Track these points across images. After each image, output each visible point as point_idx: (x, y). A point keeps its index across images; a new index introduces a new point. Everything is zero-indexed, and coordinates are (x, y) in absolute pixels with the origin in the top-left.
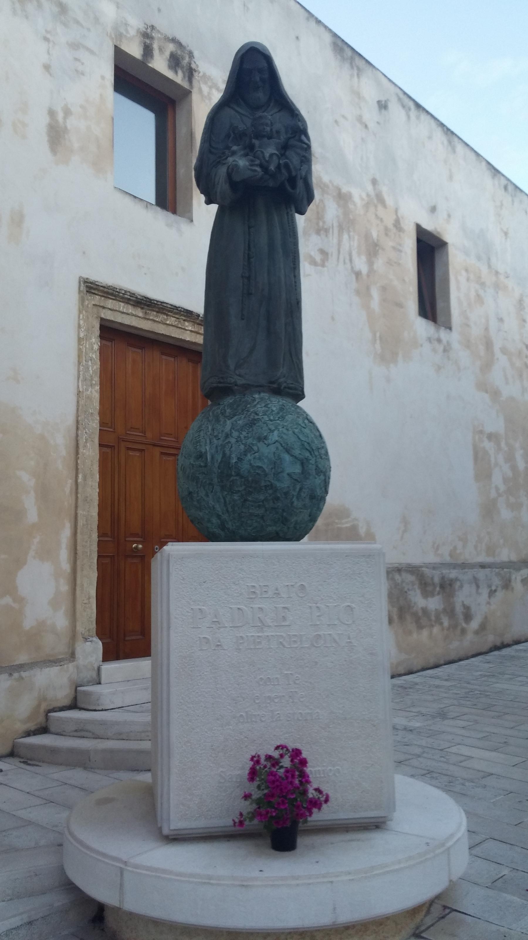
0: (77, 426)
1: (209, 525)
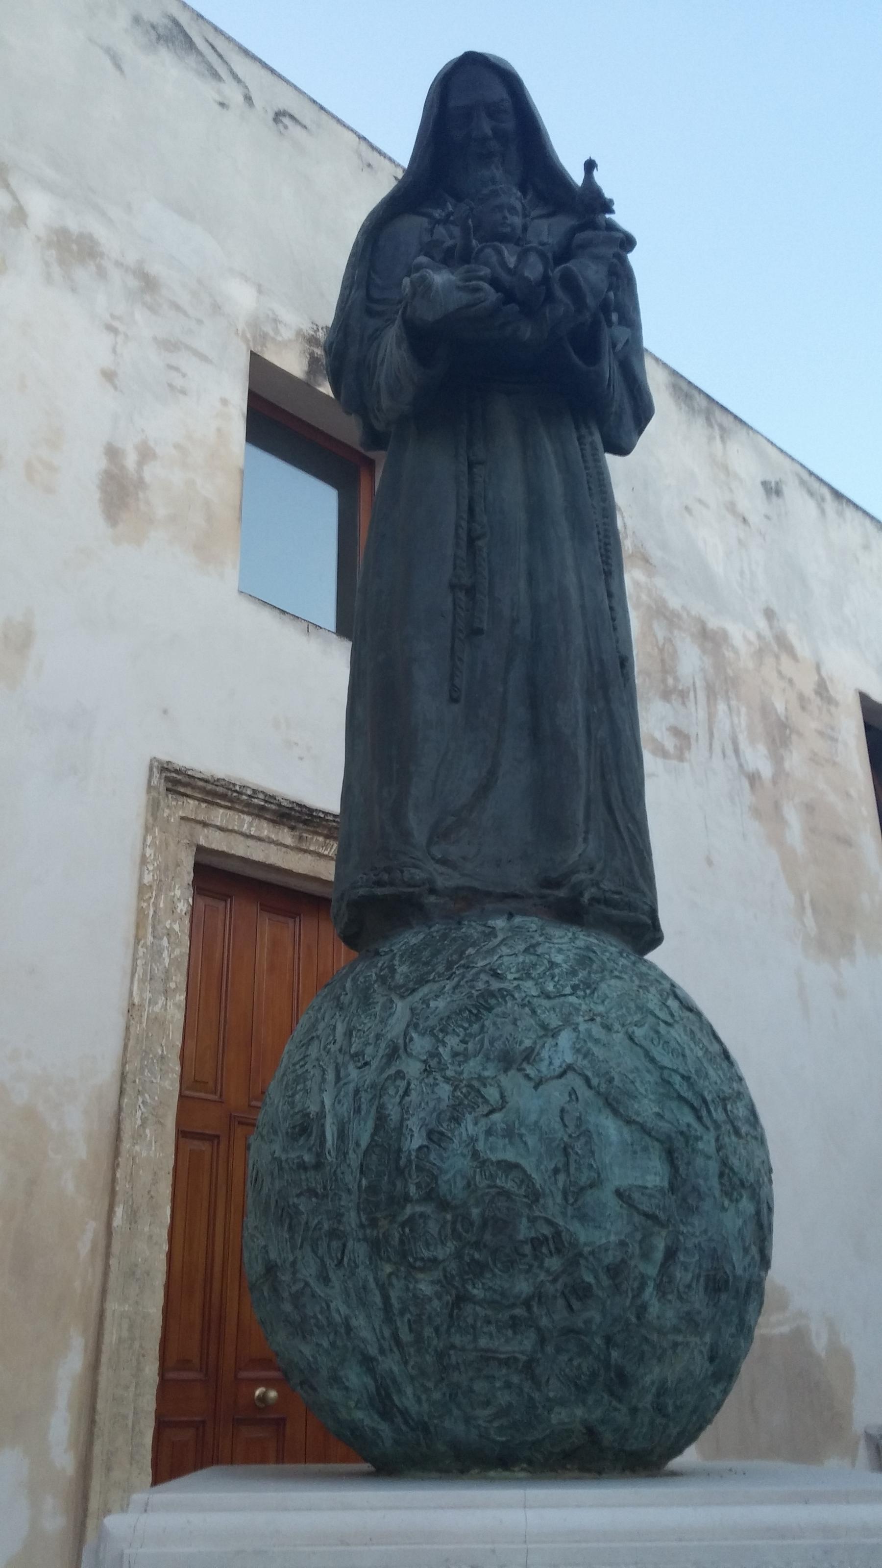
0: (121, 1087)
1: (336, 1395)
